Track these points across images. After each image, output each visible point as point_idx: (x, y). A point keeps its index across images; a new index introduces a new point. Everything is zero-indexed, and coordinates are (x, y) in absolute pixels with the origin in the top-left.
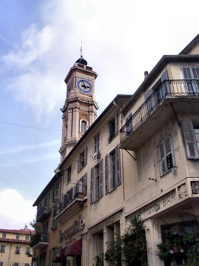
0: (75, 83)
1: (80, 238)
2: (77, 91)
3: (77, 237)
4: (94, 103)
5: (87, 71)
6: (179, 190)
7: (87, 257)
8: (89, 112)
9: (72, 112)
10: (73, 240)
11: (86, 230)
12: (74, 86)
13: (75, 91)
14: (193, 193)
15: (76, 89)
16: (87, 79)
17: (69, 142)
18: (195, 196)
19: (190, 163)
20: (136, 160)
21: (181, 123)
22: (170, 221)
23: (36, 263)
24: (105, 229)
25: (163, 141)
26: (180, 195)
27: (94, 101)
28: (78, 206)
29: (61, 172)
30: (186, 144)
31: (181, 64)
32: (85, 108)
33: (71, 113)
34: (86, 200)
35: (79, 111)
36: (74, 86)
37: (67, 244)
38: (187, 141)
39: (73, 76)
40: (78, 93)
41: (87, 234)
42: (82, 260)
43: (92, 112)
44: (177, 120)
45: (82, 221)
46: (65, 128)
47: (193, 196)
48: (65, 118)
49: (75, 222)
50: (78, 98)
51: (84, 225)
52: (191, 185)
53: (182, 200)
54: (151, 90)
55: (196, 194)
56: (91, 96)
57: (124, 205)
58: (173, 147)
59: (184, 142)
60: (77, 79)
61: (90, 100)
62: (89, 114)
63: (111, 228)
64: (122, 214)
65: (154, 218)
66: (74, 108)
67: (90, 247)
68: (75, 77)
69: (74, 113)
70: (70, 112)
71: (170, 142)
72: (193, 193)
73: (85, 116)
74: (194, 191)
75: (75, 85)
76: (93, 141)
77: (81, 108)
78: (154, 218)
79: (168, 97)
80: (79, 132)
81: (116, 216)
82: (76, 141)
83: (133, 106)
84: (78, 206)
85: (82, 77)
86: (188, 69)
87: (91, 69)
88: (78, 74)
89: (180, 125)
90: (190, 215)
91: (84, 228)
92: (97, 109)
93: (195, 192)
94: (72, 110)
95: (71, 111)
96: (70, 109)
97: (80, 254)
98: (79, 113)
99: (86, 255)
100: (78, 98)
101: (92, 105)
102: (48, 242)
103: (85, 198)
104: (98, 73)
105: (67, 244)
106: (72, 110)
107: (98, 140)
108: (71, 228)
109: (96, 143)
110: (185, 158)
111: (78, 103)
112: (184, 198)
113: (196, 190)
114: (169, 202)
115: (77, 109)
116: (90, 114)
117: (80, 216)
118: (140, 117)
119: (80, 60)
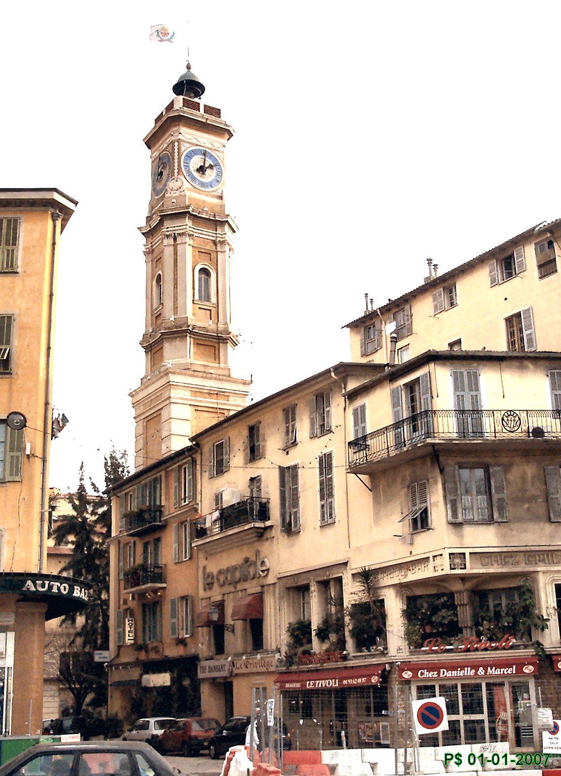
0: (179, 159)
1: (259, 589)
2: (186, 185)
3: (252, 588)
4: (229, 219)
5: (209, 124)
6: (434, 561)
7: (276, 624)
8: (215, 243)
9: (175, 246)
10: (242, 591)
11: (271, 579)
12: (176, 171)
13: (179, 183)
14: (451, 569)
15: (182, 178)
16: (210, 146)
17: (169, 328)
18: (453, 572)
19: (450, 527)
20: (371, 491)
21: (444, 469)
22: (418, 592)
23: (132, 621)
24: (313, 585)
25: (416, 484)
26: (435, 567)
27: (228, 215)
28: (255, 534)
29: (194, 447)
30: (448, 502)
31: (451, 364)
32: (207, 233)
33: (172, 248)
34: (271, 527)
35: (191, 242)
36: (176, 171)
37: (224, 595)
38: (449, 497)
39: (173, 138)
40: (188, 189)
41: (275, 588)
42: (264, 627)
43: (223, 243)
44: (438, 463)
45: (263, 563)
46: (154, 283)
47: (451, 572)
48: (153, 256)
49: (247, 560)
50: (188, 207)
51: (268, 570)
52: (450, 558)
53: (436, 574)
54: (402, 388)
55: (454, 569)
56: (221, 198)
57: (350, 555)
58: (430, 498)
59: (445, 497)
60: (183, 148)
61: (217, 209)
62: (216, 249)
63: (324, 585)
64: (346, 569)
65: (401, 588)
66: (179, 234)
67: (282, 606)
68: (179, 141)
69: (178, 246)
70: (169, 245)
71: (427, 489)
72: (451, 569)
73: (207, 255)
74: (452, 565)
75: (179, 165)
76: (280, 415)
77: (196, 235)
78: (401, 588)
79: (429, 440)
80: (193, 301)
81: (335, 570)
82: (189, 326)
83: (368, 393)
84: (255, 534)
85: (196, 142)
86: (462, 373)
87: (217, 112)
88: (187, 134)
89: (442, 471)
90: (445, 587)
91: (268, 573)
92: (234, 232)
93: (454, 567)
94: (175, 239)
95: (171, 241)
96: (168, 236)
97: (258, 616)
98: (193, 247)
99: (273, 620)
100: (188, 207)
101: (222, 223)
102: (166, 583)
103: (268, 523)
104: (233, 127)
105: (224, 595)
106: (175, 239)
107: (294, 420)
108: (235, 568)
109: (287, 422)
110: (444, 520)
111: (188, 221)
112: (440, 573)
113: (454, 565)
114: (420, 571)
115: (187, 239)
116: (219, 249)
117: (257, 553)
118: (385, 443)
119: (183, 81)
